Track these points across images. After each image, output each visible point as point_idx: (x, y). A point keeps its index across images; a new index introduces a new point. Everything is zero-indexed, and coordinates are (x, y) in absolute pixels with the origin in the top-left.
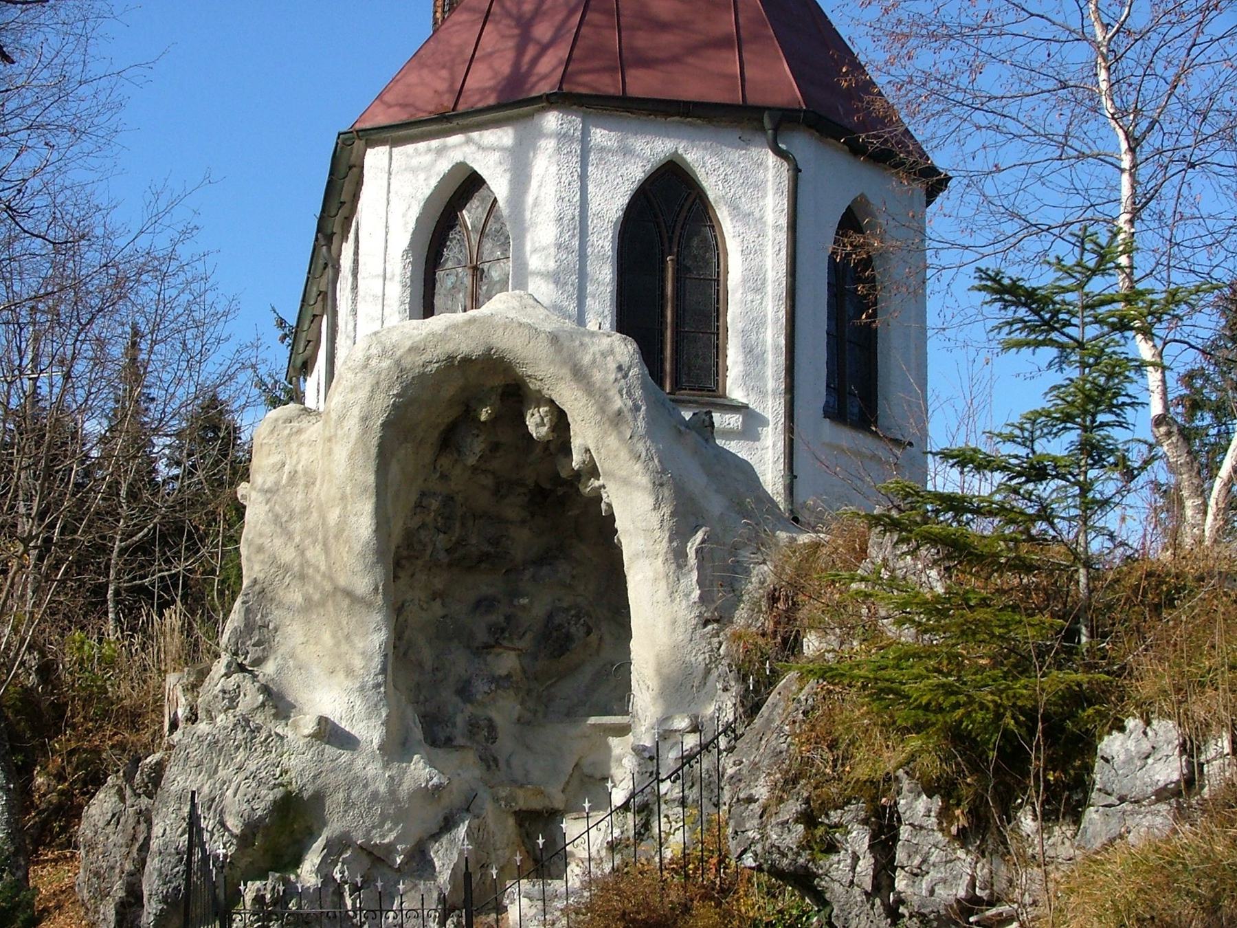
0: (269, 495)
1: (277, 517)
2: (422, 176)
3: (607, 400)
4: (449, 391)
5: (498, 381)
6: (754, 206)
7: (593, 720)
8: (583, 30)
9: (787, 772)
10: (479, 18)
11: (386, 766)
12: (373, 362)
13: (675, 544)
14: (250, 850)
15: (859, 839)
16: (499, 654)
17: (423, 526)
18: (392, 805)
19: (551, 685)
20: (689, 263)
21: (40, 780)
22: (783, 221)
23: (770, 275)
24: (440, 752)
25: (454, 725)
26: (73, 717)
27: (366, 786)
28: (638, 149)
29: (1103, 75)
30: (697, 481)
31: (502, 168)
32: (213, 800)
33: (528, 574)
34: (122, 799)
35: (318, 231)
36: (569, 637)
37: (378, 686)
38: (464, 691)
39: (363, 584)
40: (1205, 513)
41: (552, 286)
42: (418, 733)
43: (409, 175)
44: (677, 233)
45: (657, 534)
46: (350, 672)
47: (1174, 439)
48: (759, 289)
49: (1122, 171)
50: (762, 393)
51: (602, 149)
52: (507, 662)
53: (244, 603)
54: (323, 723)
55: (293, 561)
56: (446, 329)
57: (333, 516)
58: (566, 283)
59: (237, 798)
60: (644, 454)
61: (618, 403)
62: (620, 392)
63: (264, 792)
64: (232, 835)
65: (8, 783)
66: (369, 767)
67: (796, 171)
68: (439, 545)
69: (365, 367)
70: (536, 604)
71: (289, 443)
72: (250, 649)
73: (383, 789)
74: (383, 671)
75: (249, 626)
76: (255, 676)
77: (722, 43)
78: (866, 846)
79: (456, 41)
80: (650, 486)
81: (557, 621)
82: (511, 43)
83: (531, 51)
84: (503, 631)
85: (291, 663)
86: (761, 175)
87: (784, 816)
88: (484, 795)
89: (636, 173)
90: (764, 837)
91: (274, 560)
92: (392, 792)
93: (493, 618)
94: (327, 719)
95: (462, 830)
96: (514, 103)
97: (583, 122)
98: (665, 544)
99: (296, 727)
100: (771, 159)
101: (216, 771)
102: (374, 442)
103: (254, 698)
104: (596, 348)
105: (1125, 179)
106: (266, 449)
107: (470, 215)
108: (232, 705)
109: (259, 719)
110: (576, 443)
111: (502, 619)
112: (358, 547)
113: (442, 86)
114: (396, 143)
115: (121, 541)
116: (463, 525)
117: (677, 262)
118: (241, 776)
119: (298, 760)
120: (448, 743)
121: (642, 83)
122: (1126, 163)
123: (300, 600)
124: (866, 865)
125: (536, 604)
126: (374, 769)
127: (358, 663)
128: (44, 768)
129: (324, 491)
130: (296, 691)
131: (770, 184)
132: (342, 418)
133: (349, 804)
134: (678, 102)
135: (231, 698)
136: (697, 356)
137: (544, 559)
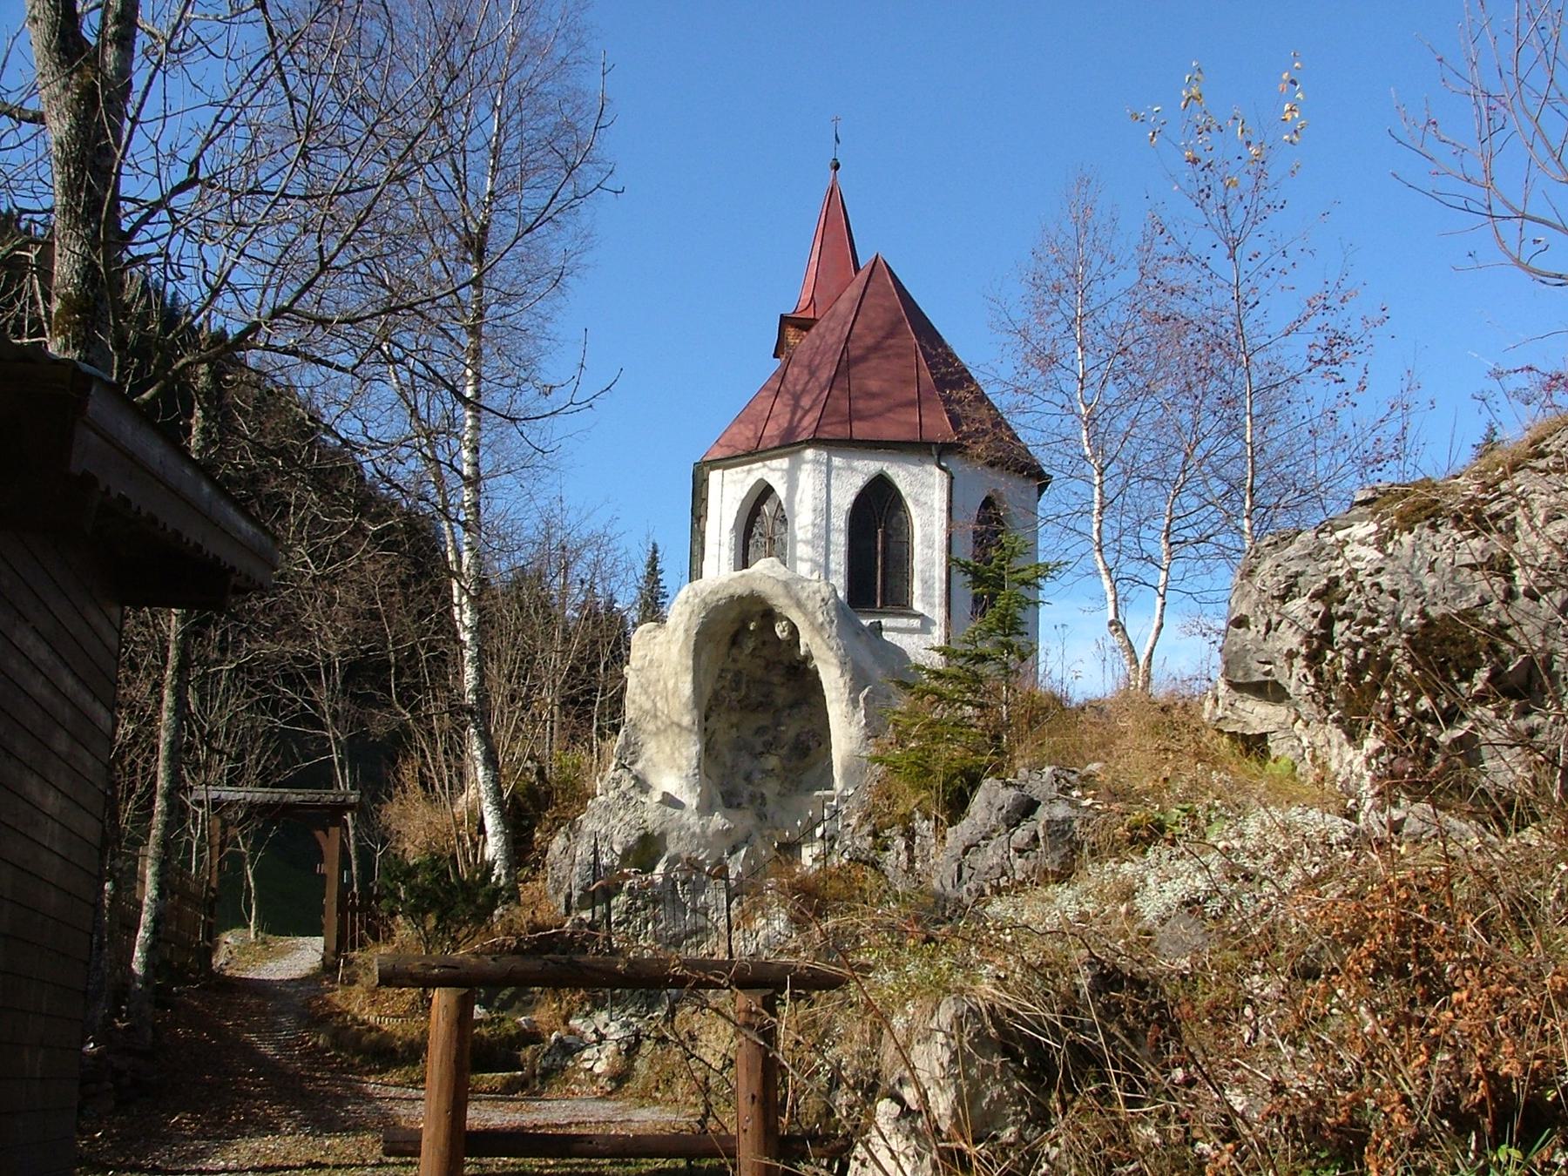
4: (733, 614)
5: (759, 608)
6: (926, 496)
15: (900, 843)
18: (704, 840)
23: (937, 538)
30: (868, 661)
36: (809, 748)
38: (748, 778)
39: (686, 720)
42: (719, 800)
46: (679, 769)
50: (932, 605)
52: (772, 762)
57: (671, 684)
59: (621, 837)
61: (820, 619)
66: (691, 819)
67: (952, 478)
75: (627, 744)
77: (910, 404)
79: (759, 408)
89: (859, 482)
92: (703, 832)
95: (743, 852)
96: (789, 445)
105: (1097, 490)
107: (767, 509)
110: (802, 641)
113: (750, 434)
114: (726, 468)
117: (885, 534)
119: (652, 814)
120: (739, 805)
121: (861, 430)
122: (1097, 481)
124: (904, 857)
126: (693, 819)
127: (684, 763)
129: (667, 670)
130: (652, 779)
132: (675, 630)
133: (679, 838)
135: (618, 782)
137: (794, 705)
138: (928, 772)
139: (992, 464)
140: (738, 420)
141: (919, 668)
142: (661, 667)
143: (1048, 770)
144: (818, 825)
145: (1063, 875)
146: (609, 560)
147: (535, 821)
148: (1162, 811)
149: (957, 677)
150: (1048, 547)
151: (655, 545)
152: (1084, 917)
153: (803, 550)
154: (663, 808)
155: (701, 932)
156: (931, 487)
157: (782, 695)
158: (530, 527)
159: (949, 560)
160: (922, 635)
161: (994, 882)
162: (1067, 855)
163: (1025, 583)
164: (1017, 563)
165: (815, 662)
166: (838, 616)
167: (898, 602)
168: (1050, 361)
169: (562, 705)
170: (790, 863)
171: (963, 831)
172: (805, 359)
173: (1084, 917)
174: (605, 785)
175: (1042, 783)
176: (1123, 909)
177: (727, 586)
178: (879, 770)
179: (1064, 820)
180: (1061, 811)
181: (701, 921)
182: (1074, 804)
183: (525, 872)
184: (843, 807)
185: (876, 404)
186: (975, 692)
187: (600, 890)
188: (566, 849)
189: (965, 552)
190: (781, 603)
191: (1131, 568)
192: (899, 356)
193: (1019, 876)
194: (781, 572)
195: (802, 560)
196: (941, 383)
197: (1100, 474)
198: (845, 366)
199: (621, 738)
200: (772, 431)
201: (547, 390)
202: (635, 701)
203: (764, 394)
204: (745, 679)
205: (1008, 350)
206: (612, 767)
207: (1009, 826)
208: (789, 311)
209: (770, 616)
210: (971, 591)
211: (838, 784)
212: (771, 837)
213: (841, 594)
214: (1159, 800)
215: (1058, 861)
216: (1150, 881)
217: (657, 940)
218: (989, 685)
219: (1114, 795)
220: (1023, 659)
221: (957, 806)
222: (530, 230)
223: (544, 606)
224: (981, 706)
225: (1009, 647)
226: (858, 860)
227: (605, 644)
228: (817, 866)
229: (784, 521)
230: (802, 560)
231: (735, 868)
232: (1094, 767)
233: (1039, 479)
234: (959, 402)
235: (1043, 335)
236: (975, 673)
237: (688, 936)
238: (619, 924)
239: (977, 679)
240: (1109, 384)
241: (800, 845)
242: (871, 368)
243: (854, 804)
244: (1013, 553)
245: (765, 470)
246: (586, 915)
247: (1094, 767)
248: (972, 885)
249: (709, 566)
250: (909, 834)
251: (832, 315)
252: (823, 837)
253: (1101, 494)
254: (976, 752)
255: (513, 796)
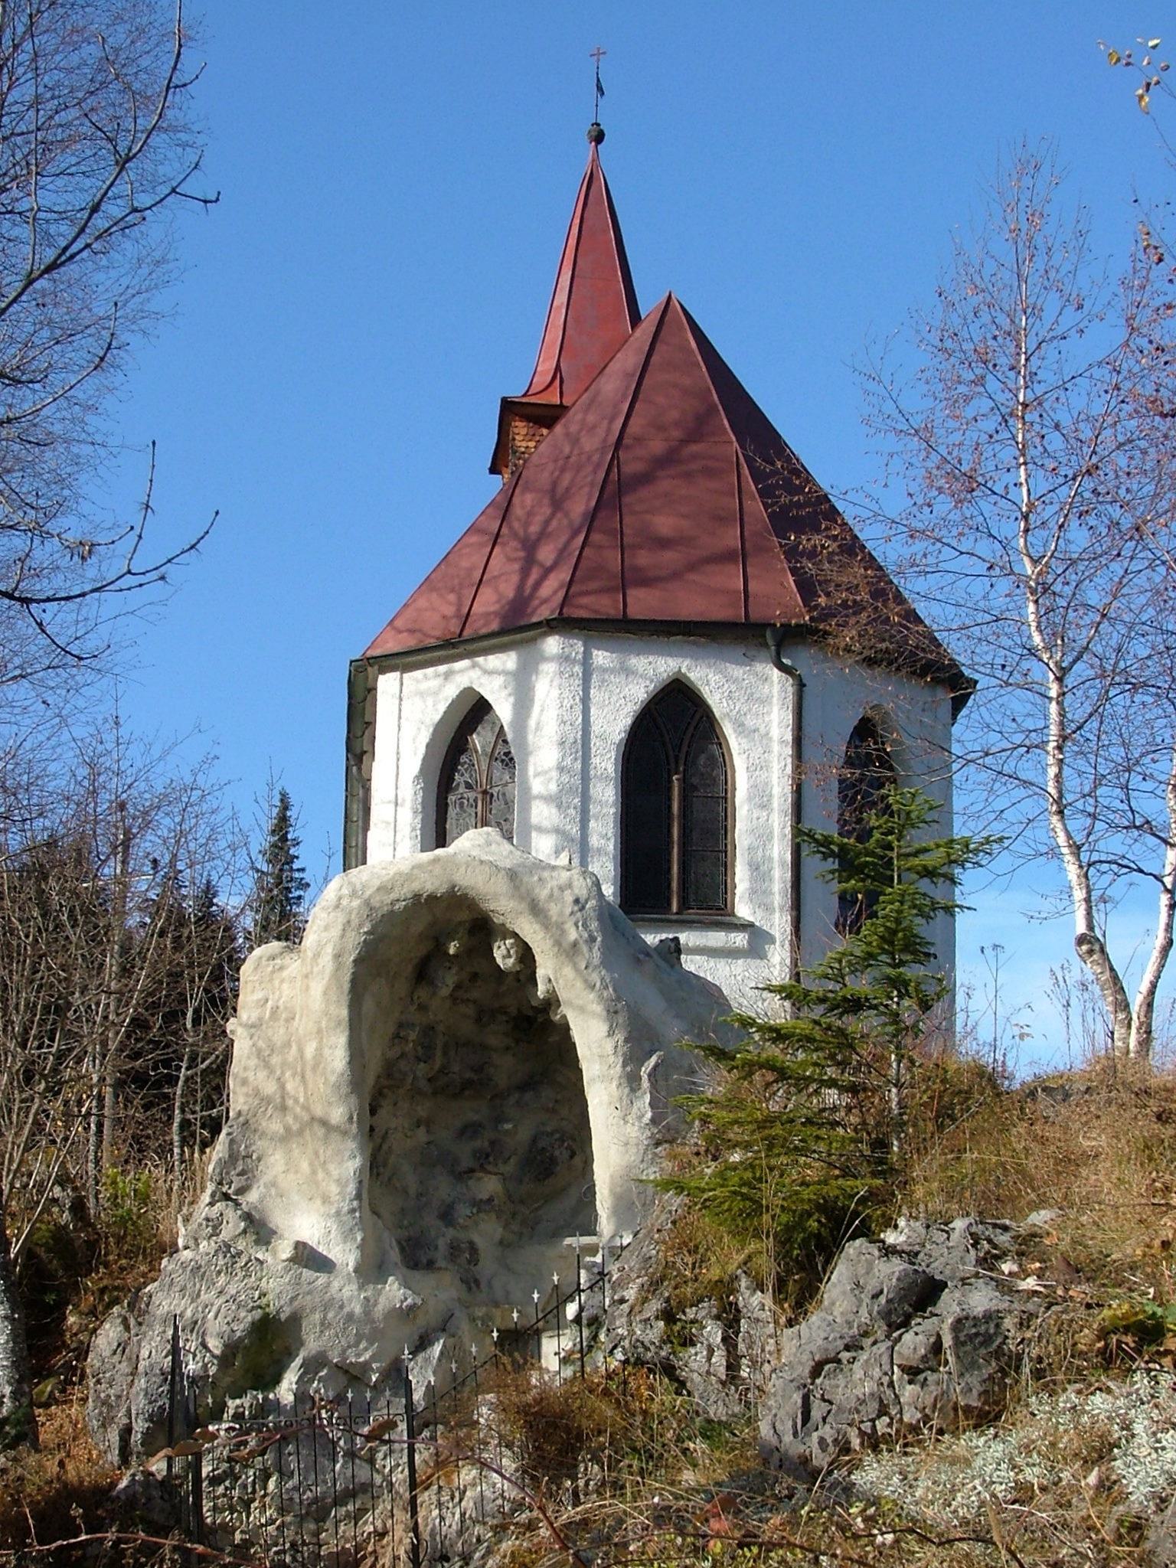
0: (253, 1030)
1: (259, 1052)
2: (430, 701)
3: (563, 932)
4: (419, 926)
5: (464, 916)
6: (757, 717)
7: (568, 1241)
8: (587, 552)
9: (654, 1274)
10: (488, 539)
11: (361, 1288)
12: (344, 902)
13: (628, 1069)
14: (231, 1371)
15: (713, 1332)
16: (479, 1179)
17: (403, 1055)
18: (369, 1327)
19: (537, 1209)
20: (695, 781)
21: (71, 1319)
22: (789, 737)
23: (776, 791)
24: (417, 1275)
25: (436, 1248)
26: (106, 1255)
27: (341, 1307)
28: (641, 670)
29: (1032, 608)
30: (654, 1007)
31: (506, 692)
32: (196, 1322)
33: (512, 1100)
34: (127, 1328)
35: (348, 751)
36: (553, 1160)
37: (353, 1211)
38: (447, 1215)
39: (338, 1114)
40: (1129, 1026)
41: (554, 811)
42: (395, 1255)
43: (417, 700)
44: (685, 749)
45: (612, 1059)
46: (326, 1200)
47: (1095, 957)
48: (765, 806)
49: (1050, 699)
50: (768, 909)
51: (605, 670)
52: (489, 1186)
53: (229, 1134)
54: (301, 1247)
55: (275, 1093)
56: (413, 868)
57: (310, 1050)
58: (569, 807)
60: (598, 984)
61: (573, 935)
62: (576, 925)
63: (243, 1314)
64: (213, 1356)
65: (13, 1313)
66: (345, 1289)
67: (800, 686)
68: (419, 1074)
69: (337, 907)
70: (519, 1130)
71: (271, 980)
72: (234, 1179)
73: (358, 1310)
74: (358, 1196)
75: (233, 1157)
76: (237, 1204)
77: (726, 557)
78: (719, 1339)
79: (465, 564)
80: (605, 1013)
81: (541, 1144)
82: (517, 566)
83: (535, 575)
84: (488, 1156)
85: (273, 1191)
86: (766, 690)
87: (647, 1314)
88: (460, 1315)
90: (632, 1333)
91: (257, 1092)
92: (367, 1312)
93: (478, 1144)
94: (305, 1244)
95: (437, 1349)
96: (516, 629)
97: (585, 645)
98: (619, 1068)
99: (275, 1254)
100: (776, 673)
101: (198, 1295)
102: (348, 977)
103: (237, 1226)
104: (555, 883)
105: (1053, 708)
106: (249, 985)
107: (479, 741)
108: (216, 1232)
109: (241, 1245)
110: (541, 973)
111: (486, 1144)
112: (333, 1079)
113: (450, 611)
115: (187, 1069)
116: (445, 1054)
117: (684, 781)
118: (222, 1299)
119: (275, 1282)
120: (430, 1265)
121: (642, 603)
123: (282, 1131)
124: (719, 1358)
125: (519, 1130)
127: (334, 1189)
128: (76, 1306)
129: (303, 1025)
130: (277, 1219)
131: (775, 700)
132: (317, 955)
133: (325, 1325)
134: (675, 622)
135: (215, 1225)
136: (705, 875)
137: (528, 1085)
138: (758, 1209)
139: (870, 662)
140: (429, 584)
141: (746, 1023)
142: (293, 1019)
143: (959, 1224)
144: (570, 1298)
145: (987, 1415)
146: (203, 832)
147: (68, 1294)
148: (1159, 1299)
149: (810, 1039)
150: (971, 806)
151: (284, 799)
152: (1023, 1493)
153: (542, 813)
154: (296, 1269)
155: (361, 1493)
156: (765, 701)
157: (506, 1067)
158: (61, 772)
159: (797, 832)
160: (749, 963)
161: (867, 1427)
162: (993, 1379)
163: (929, 873)
164: (918, 838)
165: (564, 1010)
166: (603, 928)
167: (709, 903)
168: (969, 484)
169: (119, 1085)
170: (518, 1368)
171: (816, 1330)
172: (544, 479)
173: (1023, 1493)
174: (193, 1229)
175: (949, 1251)
176: (1092, 1479)
177: (408, 877)
178: (675, 1202)
179: (988, 1316)
180: (981, 1299)
181: (363, 1473)
182: (1005, 1287)
183: (48, 1387)
184: (613, 1268)
185: (670, 558)
186: (843, 1065)
187: (179, 1418)
188: (122, 1346)
189: (825, 821)
190: (504, 907)
191: (1114, 844)
192: (709, 473)
193: (910, 1416)
194: (502, 852)
195: (540, 830)
196: (782, 522)
197: (1059, 680)
198: (614, 492)
199: (220, 1148)
200: (488, 603)
201: (85, 550)
202: (246, 1082)
203: (474, 539)
204: (440, 1042)
205: (897, 464)
206: (206, 1198)
207: (892, 1327)
208: (516, 392)
209: (483, 929)
210: (836, 887)
211: (606, 1224)
212: (487, 1319)
213: (609, 890)
214: (1154, 1279)
215: (977, 1388)
216: (1138, 1428)
217: (282, 1511)
218: (865, 1051)
219: (1076, 1270)
220: (925, 1006)
221: (799, 1288)
222: (49, 269)
223: (88, 913)
224: (853, 1089)
225: (900, 985)
226: (639, 1362)
227: (195, 972)
228: (568, 1372)
229: (508, 761)
230: (540, 830)
231: (422, 1376)
232: (1040, 1218)
233: (956, 686)
234: (812, 554)
235: (957, 438)
236: (842, 1032)
237: (338, 1501)
238: (215, 1481)
239: (845, 1041)
240: (1074, 522)
241: (538, 1333)
242: (659, 492)
243: (632, 1262)
244: (909, 822)
245: (475, 674)
246: (158, 1466)
247: (1040, 1218)
248: (827, 1432)
249: (377, 840)
250: (731, 1318)
251: (592, 401)
252: (578, 1320)
253: (1062, 714)
254: (846, 1173)
255: (28, 1252)
